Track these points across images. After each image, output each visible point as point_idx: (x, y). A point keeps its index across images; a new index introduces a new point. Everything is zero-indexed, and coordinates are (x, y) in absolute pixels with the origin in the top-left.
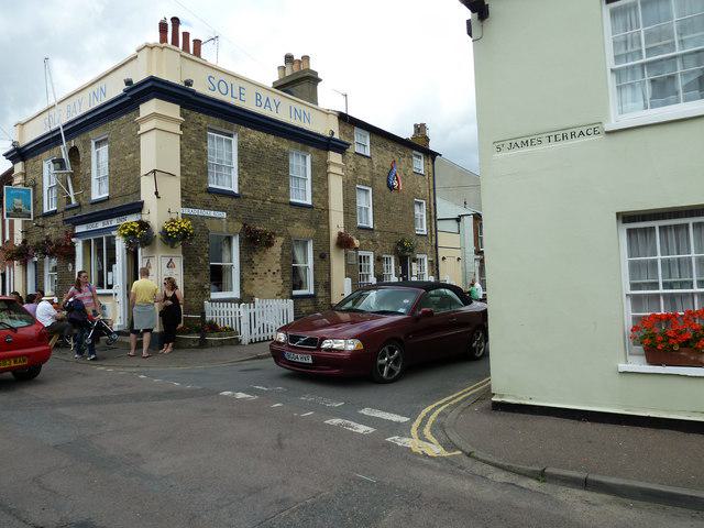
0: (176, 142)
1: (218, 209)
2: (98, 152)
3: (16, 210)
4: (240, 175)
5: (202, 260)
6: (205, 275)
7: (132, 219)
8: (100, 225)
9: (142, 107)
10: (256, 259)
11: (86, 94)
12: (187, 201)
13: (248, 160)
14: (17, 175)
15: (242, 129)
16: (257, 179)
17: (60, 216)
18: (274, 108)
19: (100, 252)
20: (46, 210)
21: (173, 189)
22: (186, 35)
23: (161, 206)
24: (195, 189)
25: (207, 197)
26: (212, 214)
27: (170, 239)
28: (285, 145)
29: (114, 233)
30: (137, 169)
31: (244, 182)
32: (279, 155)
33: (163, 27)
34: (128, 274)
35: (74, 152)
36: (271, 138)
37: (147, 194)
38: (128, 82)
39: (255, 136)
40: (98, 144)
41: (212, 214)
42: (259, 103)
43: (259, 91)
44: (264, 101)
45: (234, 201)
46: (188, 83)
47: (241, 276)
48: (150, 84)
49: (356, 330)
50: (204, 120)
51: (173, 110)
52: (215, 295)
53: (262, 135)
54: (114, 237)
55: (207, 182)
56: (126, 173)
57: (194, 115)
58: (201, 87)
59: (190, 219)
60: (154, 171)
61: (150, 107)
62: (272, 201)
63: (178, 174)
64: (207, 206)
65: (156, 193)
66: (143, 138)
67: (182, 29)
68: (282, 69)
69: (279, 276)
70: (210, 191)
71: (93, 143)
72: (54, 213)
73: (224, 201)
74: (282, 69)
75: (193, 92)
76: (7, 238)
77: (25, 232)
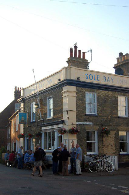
0: (75, 99)
1: (89, 121)
2: (49, 100)
3: (22, 121)
4: (98, 108)
5: (84, 140)
6: (85, 146)
7: (60, 126)
8: (50, 127)
9: (64, 88)
10: (104, 139)
11: (46, 82)
12: (78, 120)
13: (101, 102)
14: (22, 108)
15: (98, 91)
16: (105, 109)
17: (36, 123)
18: (111, 81)
19: (50, 137)
20: (31, 121)
21: (73, 116)
22: (80, 51)
23: (70, 120)
24: (81, 114)
25: (85, 117)
26: (87, 123)
27: (73, 131)
28: (115, 94)
29: (55, 131)
30: (62, 109)
31: (99, 110)
32: (114, 98)
33: (71, 50)
34: (59, 140)
35: (41, 101)
36: (110, 93)
37: (65, 117)
38: (59, 80)
39: (103, 92)
40: (49, 98)
41: (87, 123)
42: (105, 80)
43: (105, 75)
44: (107, 79)
45: (96, 118)
46: (78, 78)
47: (98, 146)
48: (66, 81)
49: (18, 139)
50: (84, 89)
51: (73, 88)
52: (88, 153)
53: (106, 92)
54: (55, 132)
55: (85, 112)
56: (58, 109)
57: (80, 89)
58: (83, 79)
59: (80, 126)
60: (67, 111)
61: (65, 89)
62: (111, 117)
63: (75, 110)
64: (86, 121)
65: (68, 118)
66: (64, 98)
67: (78, 50)
68: (118, 59)
69: (114, 146)
70: (86, 115)
71: (48, 98)
72: (35, 122)
73: (92, 118)
74: (118, 59)
75: (80, 82)
76: (17, 130)
77: (24, 128)
